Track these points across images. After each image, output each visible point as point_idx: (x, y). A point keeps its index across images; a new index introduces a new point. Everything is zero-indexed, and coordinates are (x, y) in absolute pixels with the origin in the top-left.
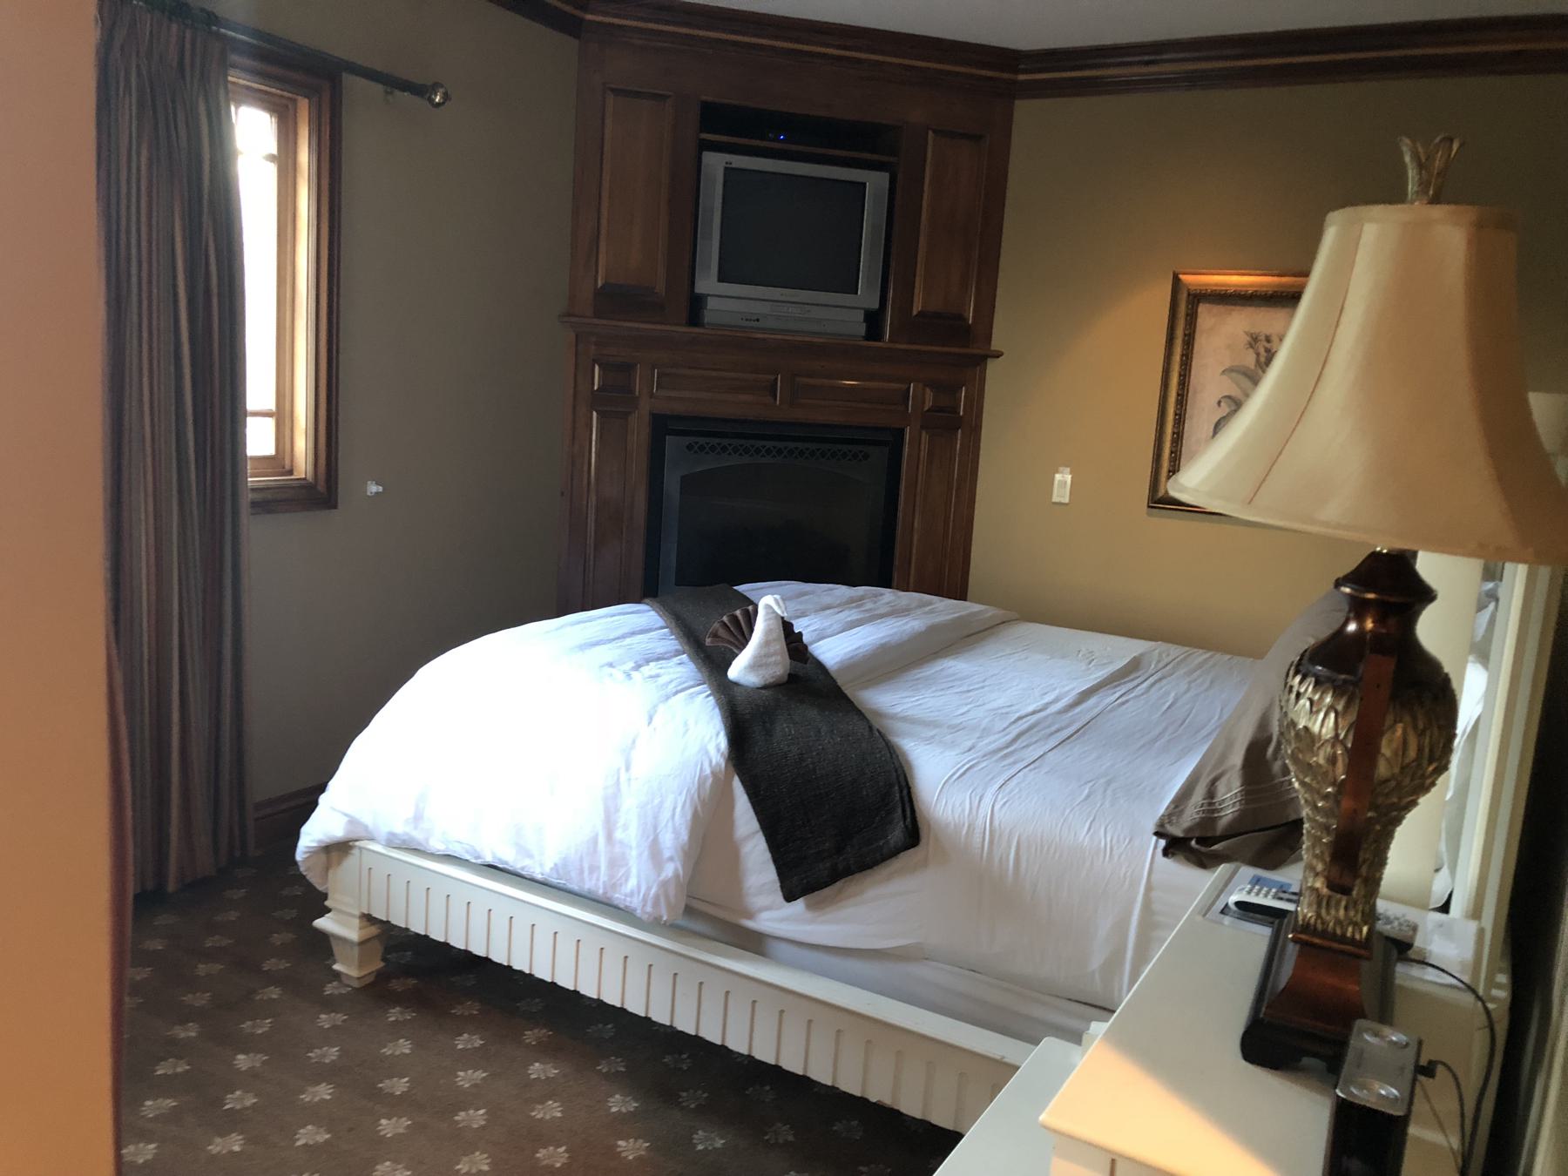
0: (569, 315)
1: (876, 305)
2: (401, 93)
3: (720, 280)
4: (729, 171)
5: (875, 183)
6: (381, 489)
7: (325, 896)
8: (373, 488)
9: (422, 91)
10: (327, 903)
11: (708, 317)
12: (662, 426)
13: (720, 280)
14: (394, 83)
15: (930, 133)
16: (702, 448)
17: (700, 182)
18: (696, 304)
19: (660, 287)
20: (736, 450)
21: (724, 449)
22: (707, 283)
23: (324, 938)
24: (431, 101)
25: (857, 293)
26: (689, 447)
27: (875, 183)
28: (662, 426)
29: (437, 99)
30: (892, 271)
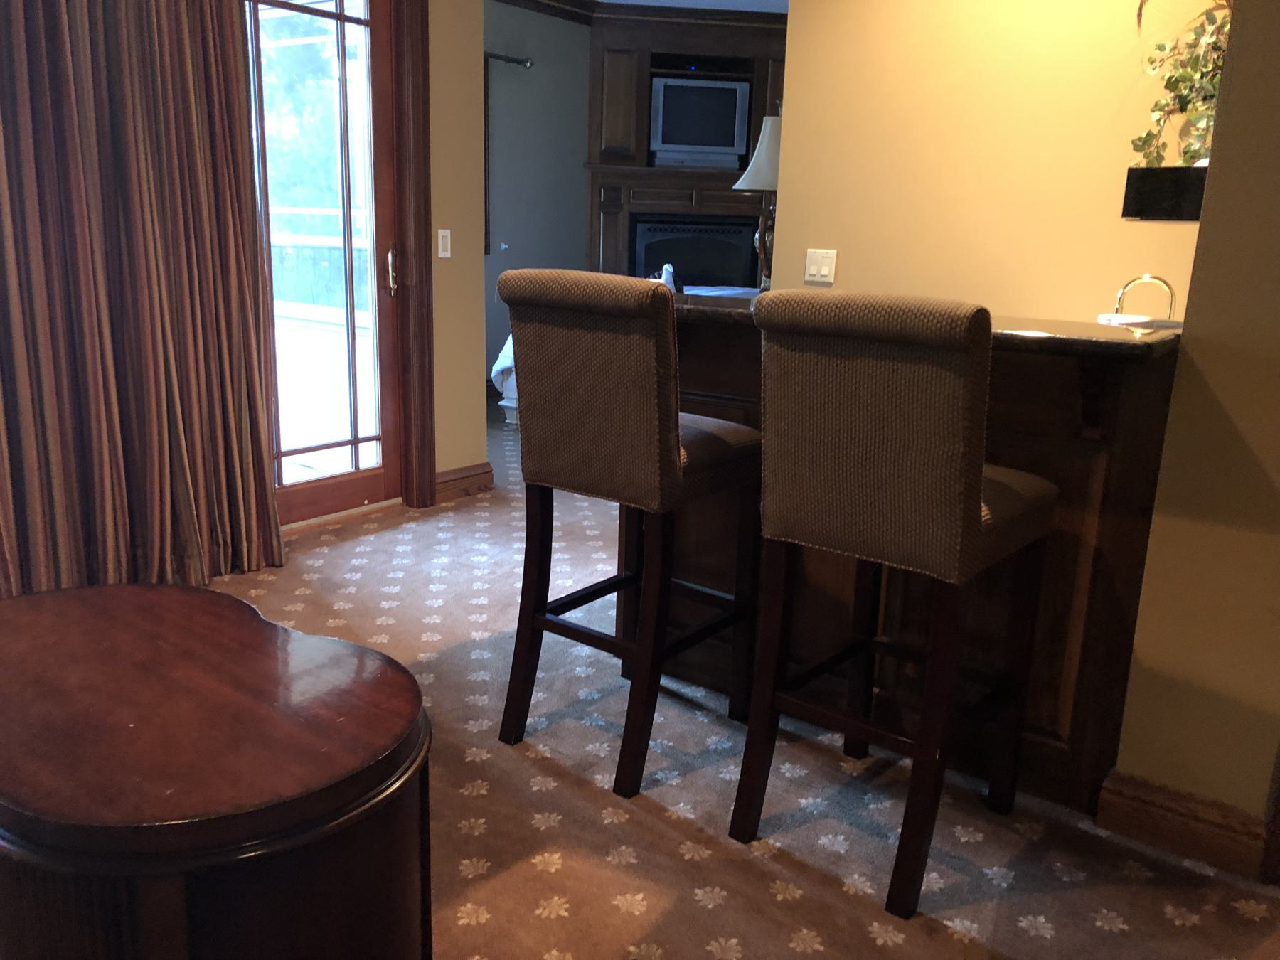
0: (589, 163)
1: (744, 152)
2: (983, 473)
3: (663, 143)
4: (667, 87)
5: (742, 89)
6: (507, 247)
7: (502, 394)
8: (504, 246)
9: (521, 62)
10: (503, 396)
11: (657, 162)
12: (635, 219)
13: (663, 143)
14: (509, 60)
15: (770, 62)
16: (655, 230)
17: (183, 419)
18: (651, 155)
19: (633, 147)
20: (672, 230)
21: (666, 230)
22: (656, 145)
23: (502, 408)
24: (525, 66)
25: (733, 146)
26: (649, 230)
27: (742, 89)
28: (635, 219)
29: (528, 65)
30: (752, 133)
